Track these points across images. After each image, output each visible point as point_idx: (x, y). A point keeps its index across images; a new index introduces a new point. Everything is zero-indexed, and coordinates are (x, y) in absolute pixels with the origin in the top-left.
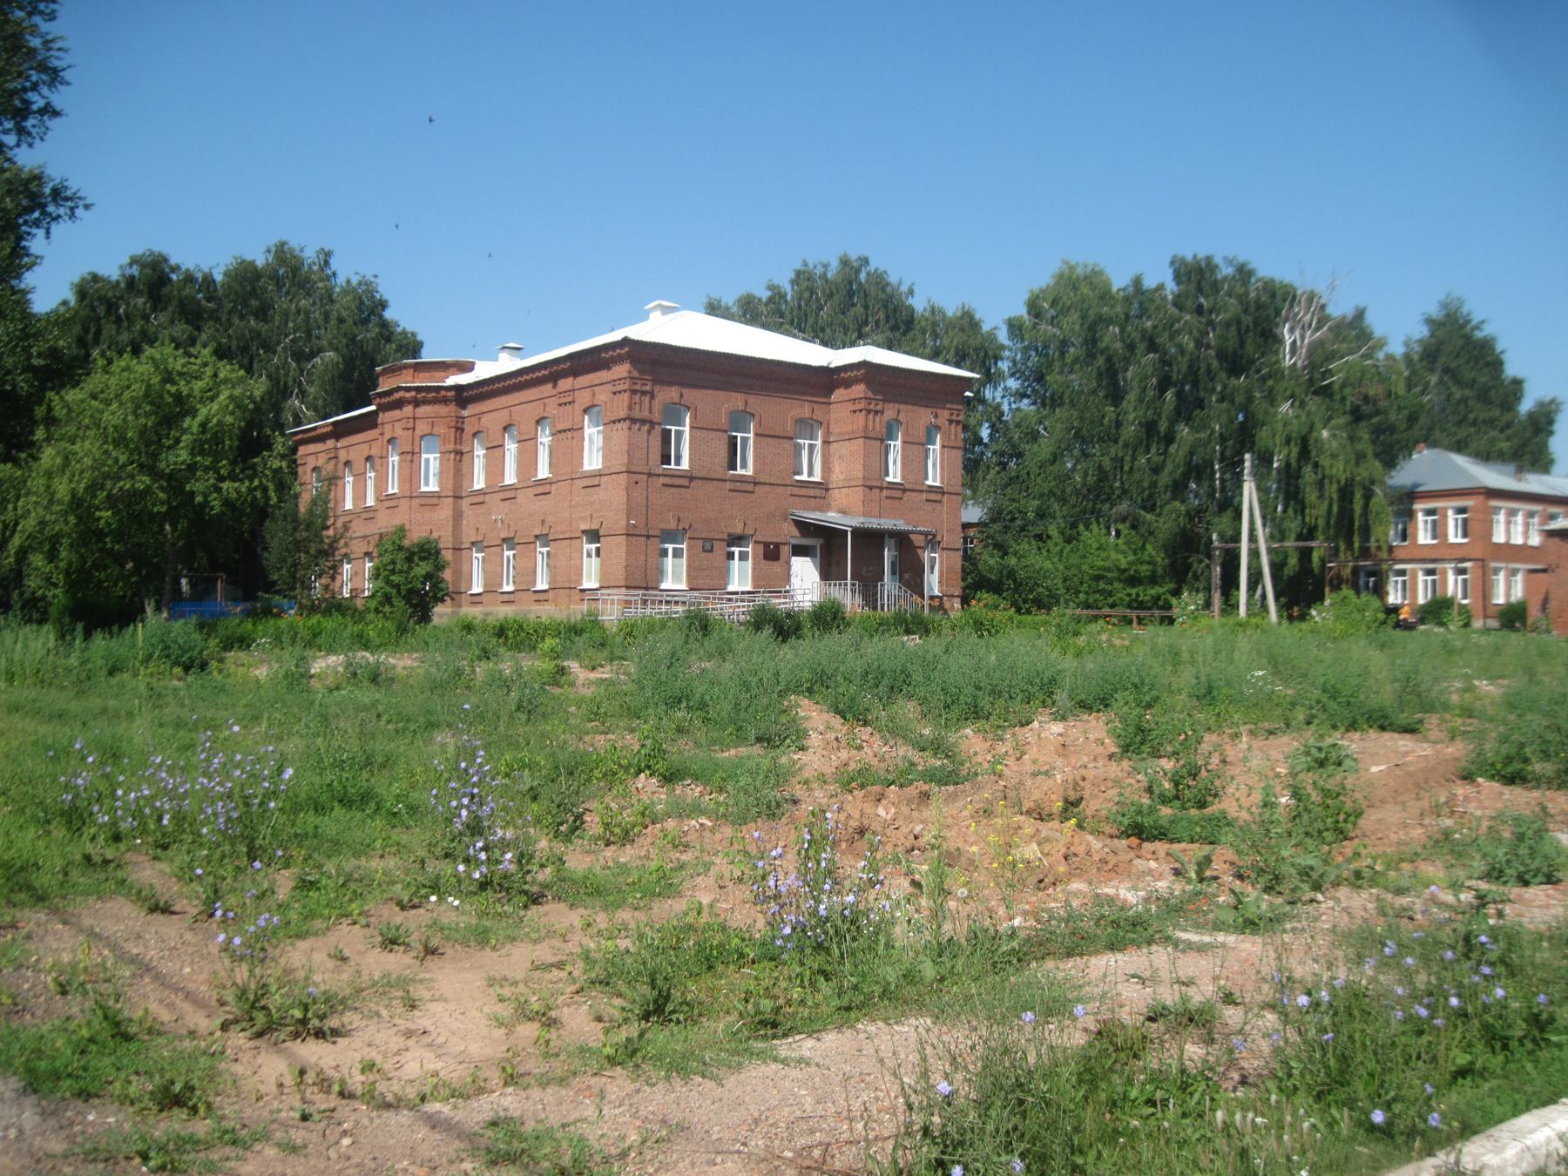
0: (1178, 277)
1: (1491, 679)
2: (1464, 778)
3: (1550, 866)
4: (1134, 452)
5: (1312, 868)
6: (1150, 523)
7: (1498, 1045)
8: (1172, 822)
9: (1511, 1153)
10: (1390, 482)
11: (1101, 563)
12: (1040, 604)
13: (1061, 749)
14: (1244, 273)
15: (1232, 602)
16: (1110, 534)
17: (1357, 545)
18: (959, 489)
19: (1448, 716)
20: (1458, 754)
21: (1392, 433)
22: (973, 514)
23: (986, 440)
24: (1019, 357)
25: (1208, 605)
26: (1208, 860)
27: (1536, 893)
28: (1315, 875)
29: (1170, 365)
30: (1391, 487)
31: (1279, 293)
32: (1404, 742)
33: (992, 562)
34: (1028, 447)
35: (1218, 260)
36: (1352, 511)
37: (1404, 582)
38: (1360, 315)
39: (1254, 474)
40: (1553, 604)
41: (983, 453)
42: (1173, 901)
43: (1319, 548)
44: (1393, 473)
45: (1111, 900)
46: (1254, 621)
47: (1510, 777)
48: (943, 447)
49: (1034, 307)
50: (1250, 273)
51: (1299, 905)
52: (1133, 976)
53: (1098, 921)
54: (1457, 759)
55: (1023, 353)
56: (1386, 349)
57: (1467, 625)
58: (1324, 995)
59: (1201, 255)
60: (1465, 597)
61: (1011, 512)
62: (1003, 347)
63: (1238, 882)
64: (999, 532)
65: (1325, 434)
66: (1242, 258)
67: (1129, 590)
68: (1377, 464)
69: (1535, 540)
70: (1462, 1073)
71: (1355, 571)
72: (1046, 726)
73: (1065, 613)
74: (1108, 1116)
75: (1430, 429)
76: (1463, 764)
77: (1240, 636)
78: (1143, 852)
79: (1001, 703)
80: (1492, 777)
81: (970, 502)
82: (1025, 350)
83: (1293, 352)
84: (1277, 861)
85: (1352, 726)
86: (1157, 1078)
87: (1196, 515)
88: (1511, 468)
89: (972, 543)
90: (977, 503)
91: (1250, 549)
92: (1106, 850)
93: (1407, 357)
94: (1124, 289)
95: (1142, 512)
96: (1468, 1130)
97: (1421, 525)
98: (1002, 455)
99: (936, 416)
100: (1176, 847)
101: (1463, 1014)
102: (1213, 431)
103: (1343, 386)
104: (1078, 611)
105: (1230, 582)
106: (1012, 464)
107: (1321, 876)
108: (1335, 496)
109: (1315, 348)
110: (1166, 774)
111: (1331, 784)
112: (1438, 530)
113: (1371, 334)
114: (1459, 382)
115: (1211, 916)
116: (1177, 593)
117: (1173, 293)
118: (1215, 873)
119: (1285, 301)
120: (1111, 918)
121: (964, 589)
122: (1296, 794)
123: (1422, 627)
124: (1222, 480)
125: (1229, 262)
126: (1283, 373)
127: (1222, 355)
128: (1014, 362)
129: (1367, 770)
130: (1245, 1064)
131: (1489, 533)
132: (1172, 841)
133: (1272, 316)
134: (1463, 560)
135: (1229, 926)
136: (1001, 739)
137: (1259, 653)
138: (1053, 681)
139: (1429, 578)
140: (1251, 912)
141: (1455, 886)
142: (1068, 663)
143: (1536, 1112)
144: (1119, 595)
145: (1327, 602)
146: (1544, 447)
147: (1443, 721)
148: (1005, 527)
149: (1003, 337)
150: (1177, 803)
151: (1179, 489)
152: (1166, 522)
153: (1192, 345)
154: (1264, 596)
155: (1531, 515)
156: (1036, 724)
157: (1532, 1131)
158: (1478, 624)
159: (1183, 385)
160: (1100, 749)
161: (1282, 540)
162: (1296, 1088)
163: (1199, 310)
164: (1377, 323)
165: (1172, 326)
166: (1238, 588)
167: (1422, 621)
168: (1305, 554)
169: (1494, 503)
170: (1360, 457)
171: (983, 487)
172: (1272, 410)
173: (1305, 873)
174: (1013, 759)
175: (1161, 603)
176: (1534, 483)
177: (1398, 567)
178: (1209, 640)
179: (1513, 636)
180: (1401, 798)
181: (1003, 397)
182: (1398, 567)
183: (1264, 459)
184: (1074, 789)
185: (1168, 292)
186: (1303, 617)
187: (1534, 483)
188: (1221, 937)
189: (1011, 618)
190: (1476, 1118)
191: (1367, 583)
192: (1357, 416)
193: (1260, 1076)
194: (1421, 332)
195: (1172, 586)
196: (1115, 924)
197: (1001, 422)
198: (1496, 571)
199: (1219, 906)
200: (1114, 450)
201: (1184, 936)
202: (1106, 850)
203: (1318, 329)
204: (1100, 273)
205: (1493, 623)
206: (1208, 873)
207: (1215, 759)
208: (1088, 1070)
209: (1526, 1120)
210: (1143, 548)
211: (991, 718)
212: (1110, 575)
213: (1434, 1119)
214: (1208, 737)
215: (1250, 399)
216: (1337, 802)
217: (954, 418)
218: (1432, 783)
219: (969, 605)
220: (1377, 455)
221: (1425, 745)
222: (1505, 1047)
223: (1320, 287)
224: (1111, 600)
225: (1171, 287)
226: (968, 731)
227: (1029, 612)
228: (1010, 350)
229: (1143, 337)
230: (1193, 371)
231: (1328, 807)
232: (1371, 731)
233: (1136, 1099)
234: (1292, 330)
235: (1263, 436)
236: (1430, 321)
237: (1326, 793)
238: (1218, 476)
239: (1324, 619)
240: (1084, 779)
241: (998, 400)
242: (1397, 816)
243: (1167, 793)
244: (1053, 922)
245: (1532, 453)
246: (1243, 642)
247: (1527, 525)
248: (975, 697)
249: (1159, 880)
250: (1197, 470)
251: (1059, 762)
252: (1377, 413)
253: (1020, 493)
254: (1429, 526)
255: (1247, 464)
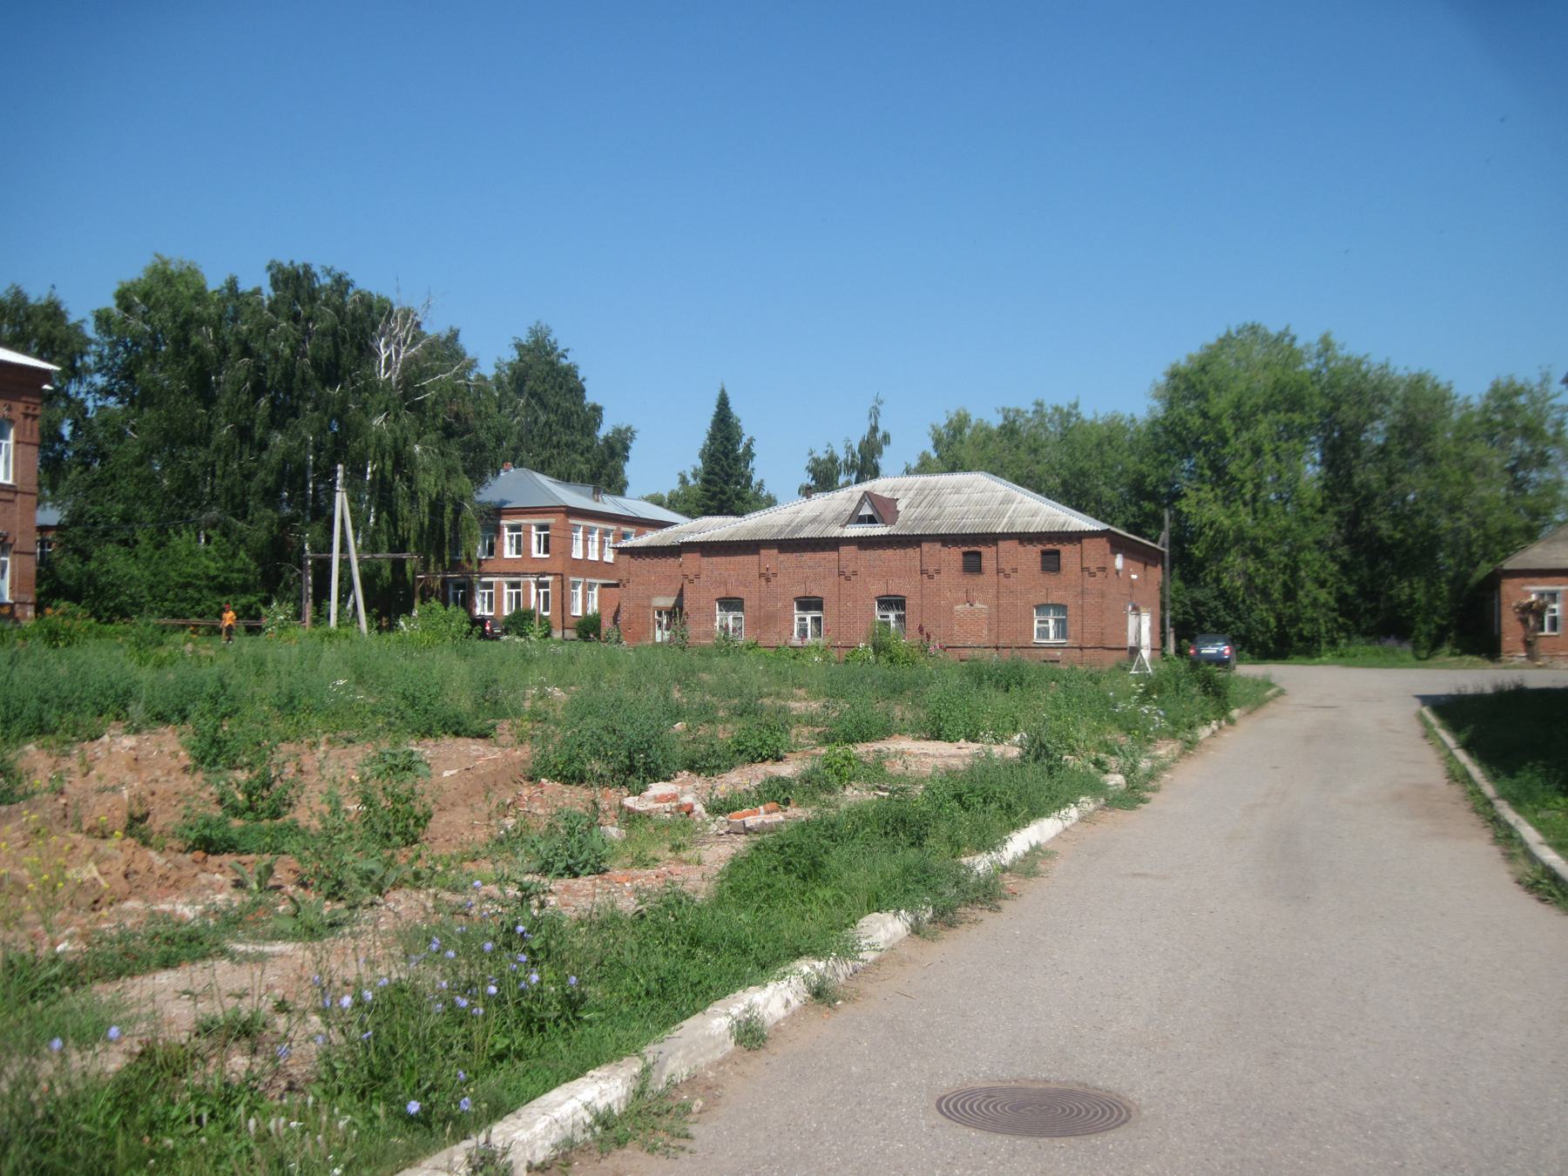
0: (275, 283)
1: (562, 687)
2: (531, 779)
3: (596, 857)
4: (226, 457)
5: (373, 872)
6: (241, 531)
7: (535, 1028)
8: (243, 834)
9: (539, 1127)
10: (478, 498)
11: (189, 570)
12: (124, 614)
13: (133, 763)
14: (341, 284)
15: (324, 613)
16: (199, 541)
17: (447, 558)
18: (35, 489)
19: (518, 721)
20: (525, 757)
21: (481, 451)
22: (51, 516)
23: (67, 438)
24: (106, 351)
25: (298, 615)
26: (270, 870)
27: (584, 883)
28: (375, 878)
29: (264, 370)
30: (479, 503)
31: (376, 306)
32: (476, 747)
33: (71, 567)
34: (113, 447)
35: (316, 269)
36: (442, 525)
37: (490, 595)
38: (454, 336)
39: (348, 485)
40: (623, 616)
41: (63, 452)
42: (231, 913)
43: (412, 560)
44: (481, 490)
45: (167, 917)
46: (343, 631)
47: (574, 778)
48: (17, 442)
49: (123, 297)
50: (349, 284)
51: (360, 909)
52: (185, 993)
53: (153, 938)
54: (524, 762)
55: (111, 349)
56: (477, 370)
57: (547, 635)
58: (368, 995)
59: (298, 262)
60: (546, 609)
61: (93, 516)
62: (89, 342)
63: (301, 890)
64: (80, 537)
65: (418, 448)
66: (339, 269)
67: (218, 599)
68: (466, 479)
69: (609, 557)
70: (501, 1057)
71: (445, 582)
72: (118, 740)
73: (148, 624)
74: (147, 1139)
75: (516, 450)
76: (530, 765)
77: (326, 644)
78: (209, 866)
79: (70, 716)
80: (554, 778)
81: (49, 504)
82: (113, 345)
83: (388, 368)
84: (340, 866)
85: (428, 733)
86: (198, 1096)
87: (286, 524)
88: (590, 489)
89: (49, 547)
90: (55, 505)
91: (341, 560)
92: (169, 865)
93: (497, 378)
94: (219, 292)
95: (234, 520)
96: (498, 1111)
97: (507, 540)
98: (85, 454)
99: (9, 409)
100: (244, 858)
101: (500, 1001)
102: (305, 440)
103: (435, 403)
104: (163, 621)
105: (322, 593)
106: (96, 465)
107: (382, 879)
108: (427, 510)
109: (409, 362)
110: (239, 786)
111: (401, 790)
112: (520, 546)
113: (465, 354)
114: (544, 406)
115: (270, 926)
116: (267, 602)
117: (269, 298)
118: (278, 883)
119: (382, 315)
120: (166, 934)
121: (39, 596)
122: (366, 800)
123: (505, 638)
124: (315, 490)
125: (329, 272)
126: (377, 386)
127: (316, 364)
128: (101, 357)
129: (440, 775)
130: (294, 1071)
131: (568, 549)
132: (241, 853)
133: (368, 330)
134: (543, 574)
135: (288, 935)
136: (67, 755)
137: (345, 663)
138: (128, 693)
139: (514, 591)
140: (312, 919)
141: (502, 881)
142: (146, 675)
143: (565, 1086)
144: (208, 603)
145: (415, 613)
146: (619, 471)
147: (513, 725)
148: (87, 531)
149: (90, 330)
150: (250, 815)
151: (270, 497)
152: (259, 527)
153: (287, 351)
154: (355, 606)
155: (606, 533)
156: (106, 738)
157: (560, 1105)
158: (557, 635)
159: (277, 392)
160: (174, 763)
161: (376, 550)
162: (340, 1090)
163: (295, 318)
164: (470, 345)
165: (268, 331)
166: (329, 600)
167: (506, 631)
168: (399, 566)
169: (573, 521)
170: (450, 472)
171: (63, 487)
172: (366, 423)
173: (366, 877)
174: (78, 776)
175: (253, 613)
176: (609, 504)
177: (484, 580)
178: (296, 650)
179: (586, 645)
180: (470, 801)
181: (88, 393)
182: (484, 580)
183: (356, 471)
184: (140, 804)
185: (265, 298)
186: (392, 627)
187: (609, 504)
188: (279, 947)
189: (90, 628)
190: (508, 1098)
191: (456, 595)
192: (448, 432)
193: (308, 1081)
194: (511, 355)
195: (263, 594)
196: (169, 940)
197: (85, 419)
198: (575, 585)
199: (278, 915)
200: (202, 454)
201: (241, 947)
202: (169, 865)
203: (412, 345)
204: (194, 272)
205: (571, 634)
206: (271, 883)
207: (290, 769)
208: (126, 1094)
209: (556, 1095)
210: (234, 555)
211: (58, 732)
212: (198, 582)
213: (466, 1104)
214: (284, 747)
215: (345, 409)
216: (407, 806)
217: (30, 411)
218: (500, 785)
219: (44, 614)
220: (466, 472)
221: (496, 749)
222: (542, 1028)
223: (416, 304)
224: (199, 609)
225: (268, 292)
226: (31, 748)
227: (110, 621)
228: (97, 344)
229: (238, 341)
230: (288, 375)
231: (398, 811)
232: (446, 737)
233: (177, 1118)
234: (387, 345)
235: (356, 446)
236: (519, 346)
237: (396, 798)
238: (311, 485)
239: (412, 629)
240: (153, 794)
241: (82, 396)
242: (466, 817)
243: (241, 806)
244: (104, 944)
245: (609, 476)
246: (328, 653)
247: (602, 543)
248: (40, 711)
249: (220, 893)
250: (290, 475)
251: (129, 778)
252: (468, 431)
253: (103, 496)
254: (514, 541)
255: (340, 475)
